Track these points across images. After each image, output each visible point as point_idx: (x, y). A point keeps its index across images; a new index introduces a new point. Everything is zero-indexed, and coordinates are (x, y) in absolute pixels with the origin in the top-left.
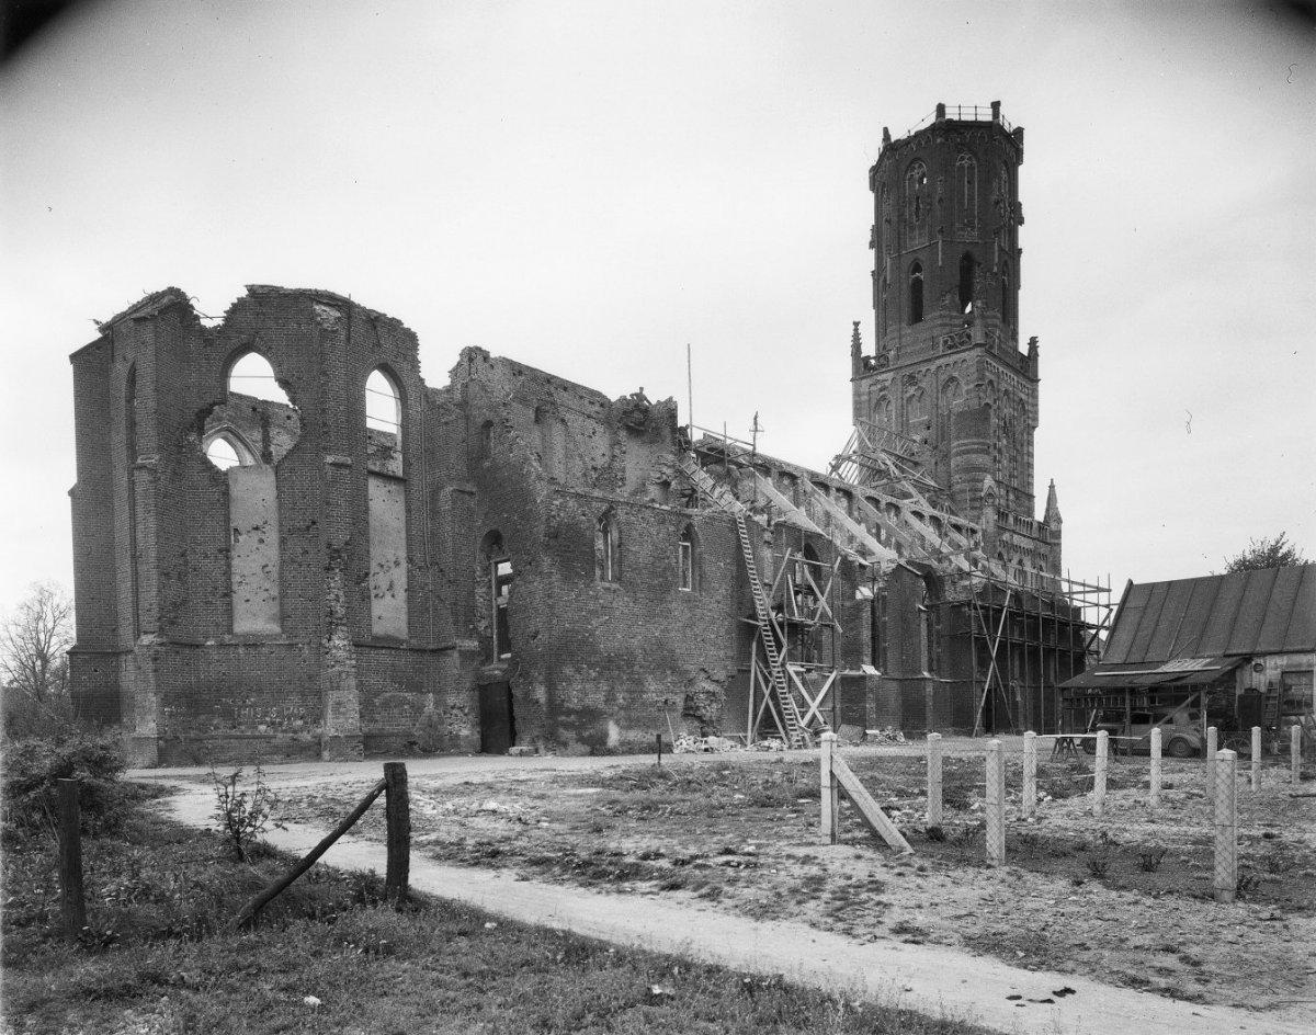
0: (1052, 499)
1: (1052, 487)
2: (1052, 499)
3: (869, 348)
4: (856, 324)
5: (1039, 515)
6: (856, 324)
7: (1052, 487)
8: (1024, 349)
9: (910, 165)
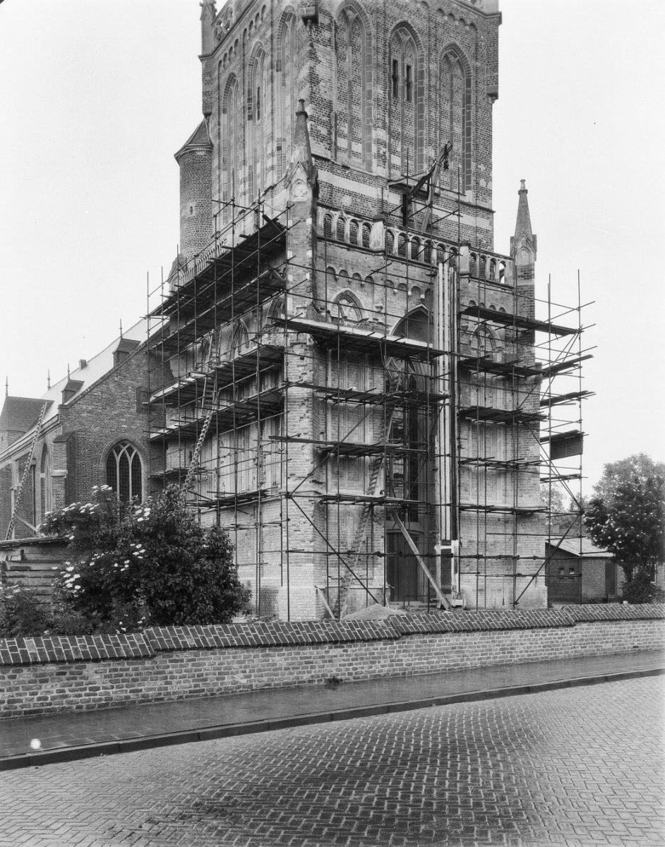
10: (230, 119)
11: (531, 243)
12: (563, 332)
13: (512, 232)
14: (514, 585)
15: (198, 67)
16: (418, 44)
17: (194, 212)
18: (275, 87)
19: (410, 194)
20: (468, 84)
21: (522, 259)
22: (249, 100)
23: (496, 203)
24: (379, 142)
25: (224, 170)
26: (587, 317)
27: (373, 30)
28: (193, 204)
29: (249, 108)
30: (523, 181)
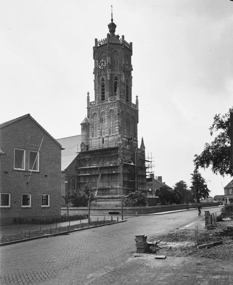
0: (137, 100)
1: (142, 139)
2: (137, 100)
3: (92, 99)
4: (88, 93)
5: (139, 147)
6: (88, 93)
7: (142, 139)
8: (134, 101)
9: (101, 53)
10: (94, 120)
11: (144, 148)
12: (148, 161)
13: (140, 145)
14: (81, 221)
15: (87, 110)
16: (129, 115)
17: (86, 135)
18: (109, 120)
19: (129, 139)
20: (135, 121)
21: (143, 150)
22: (101, 119)
23: (138, 140)
24: (125, 131)
25: (93, 128)
26: (153, 160)
27: (124, 114)
28: (86, 133)
29: (101, 121)
30: (88, 92)
